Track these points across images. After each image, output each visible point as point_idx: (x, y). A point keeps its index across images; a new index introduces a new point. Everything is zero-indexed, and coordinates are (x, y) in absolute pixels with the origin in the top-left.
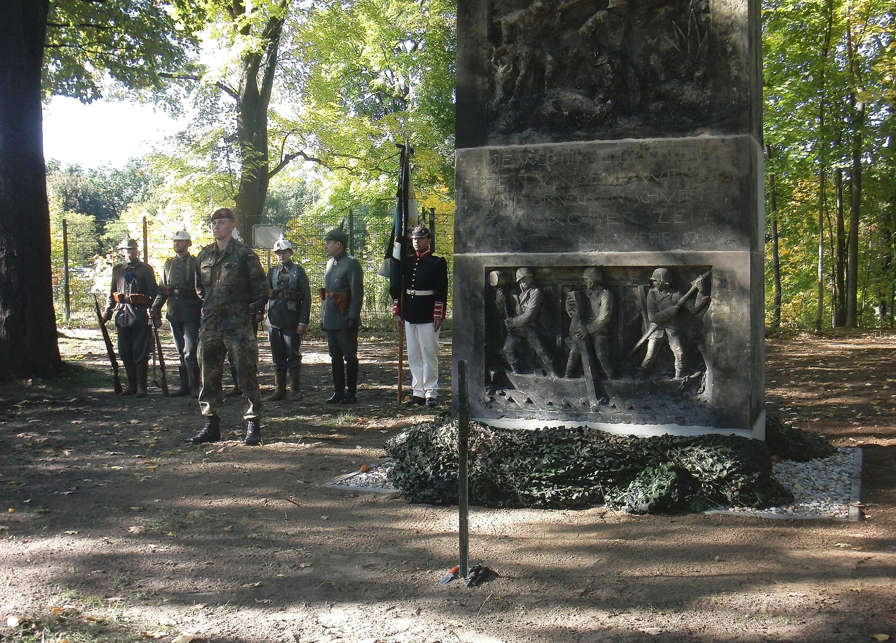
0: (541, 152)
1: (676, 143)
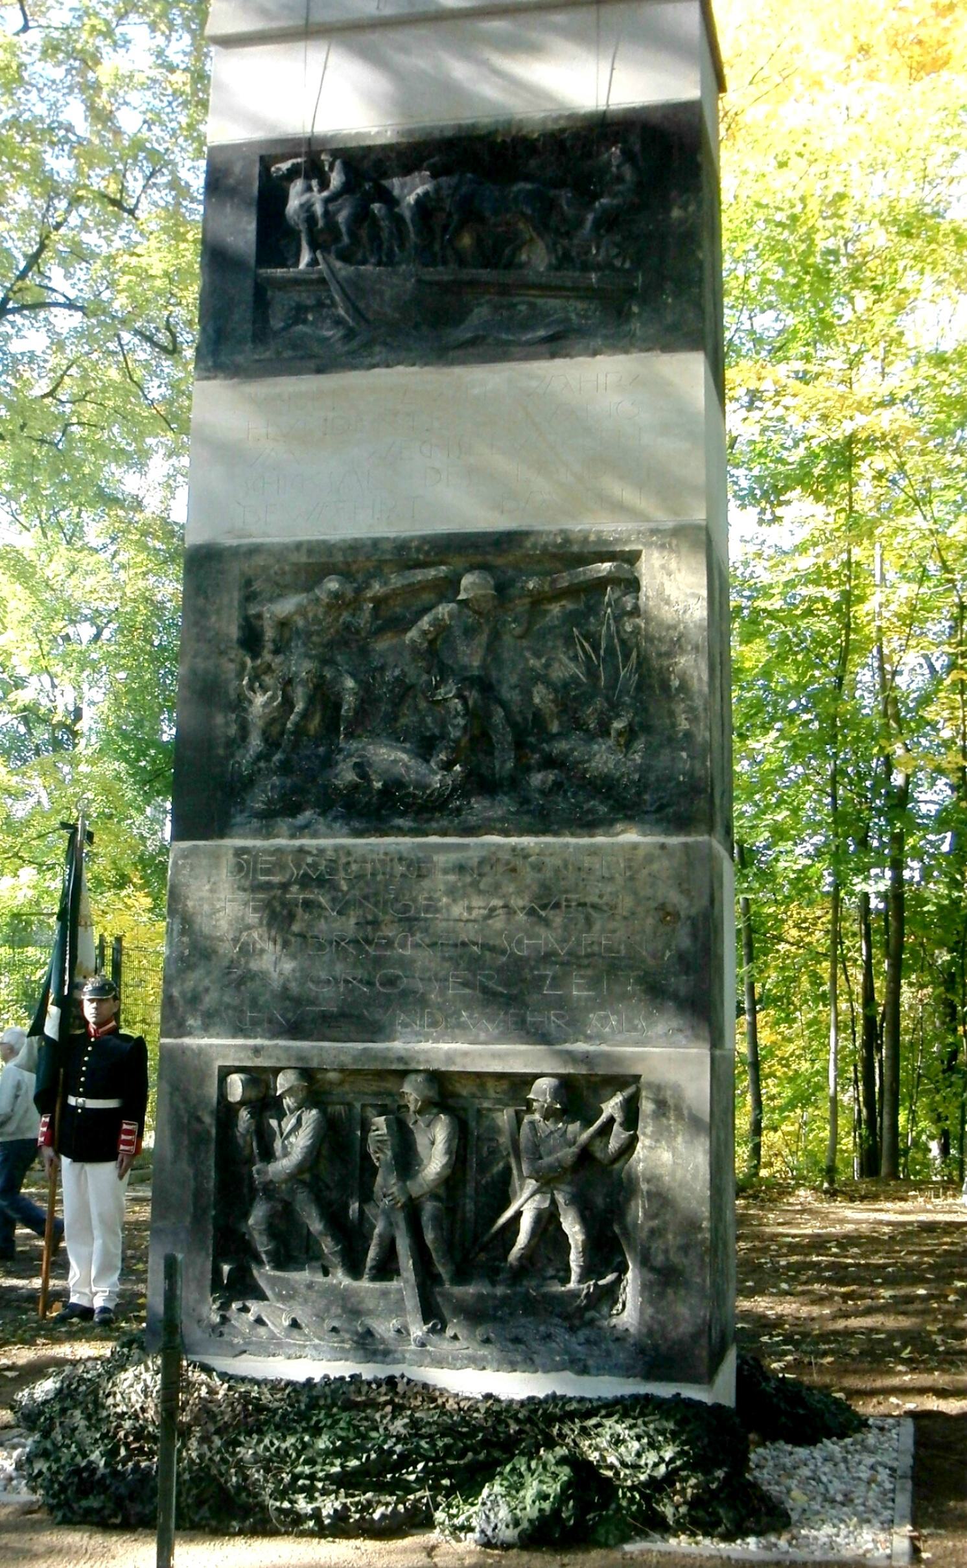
0: (330, 854)
1: (577, 847)
